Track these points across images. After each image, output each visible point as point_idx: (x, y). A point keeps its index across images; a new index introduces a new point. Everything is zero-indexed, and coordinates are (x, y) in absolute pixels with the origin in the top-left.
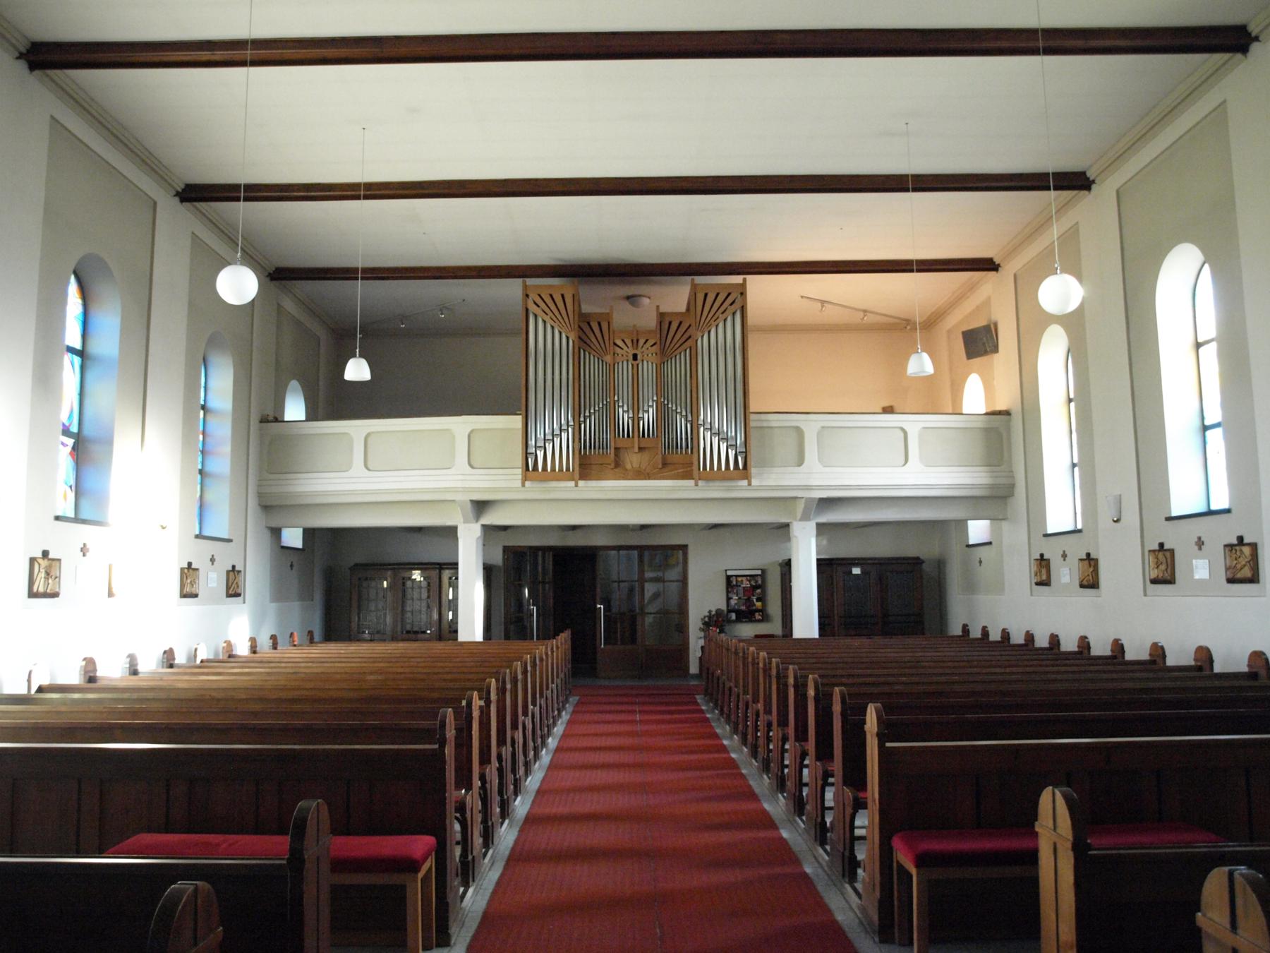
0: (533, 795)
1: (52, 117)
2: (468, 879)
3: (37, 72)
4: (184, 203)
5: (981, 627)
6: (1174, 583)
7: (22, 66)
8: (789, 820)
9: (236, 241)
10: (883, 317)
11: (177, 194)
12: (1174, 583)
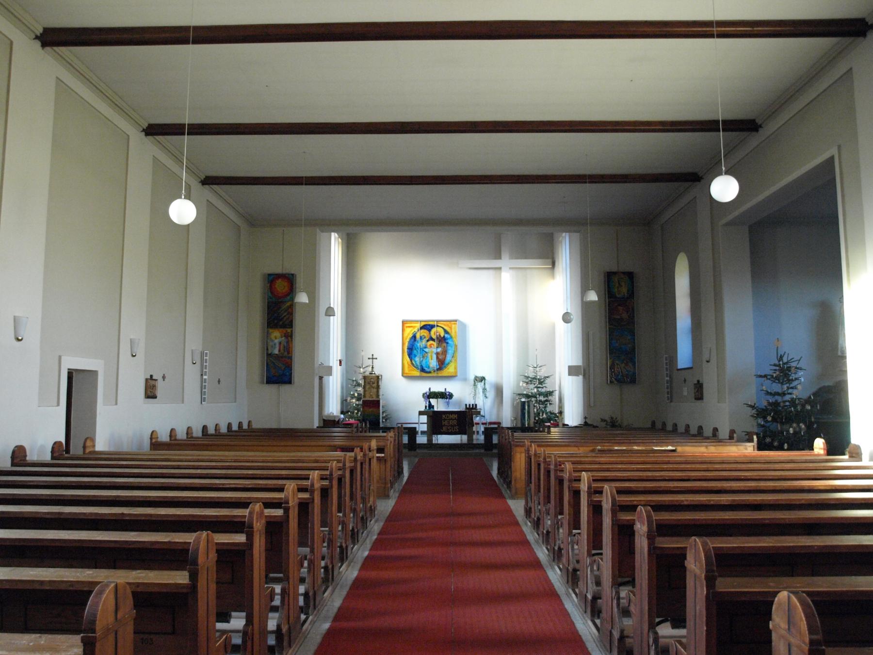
0: (347, 588)
1: (208, 200)
2: (355, 540)
3: (48, 49)
4: (148, 137)
5: (712, 429)
6: (289, 382)
7: (38, 44)
8: (567, 594)
9: (182, 160)
10: (639, 187)
11: (144, 130)
12: (289, 382)
